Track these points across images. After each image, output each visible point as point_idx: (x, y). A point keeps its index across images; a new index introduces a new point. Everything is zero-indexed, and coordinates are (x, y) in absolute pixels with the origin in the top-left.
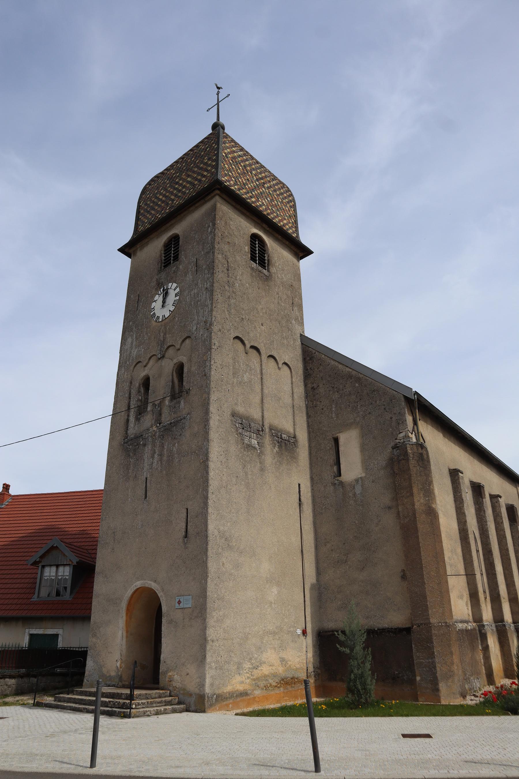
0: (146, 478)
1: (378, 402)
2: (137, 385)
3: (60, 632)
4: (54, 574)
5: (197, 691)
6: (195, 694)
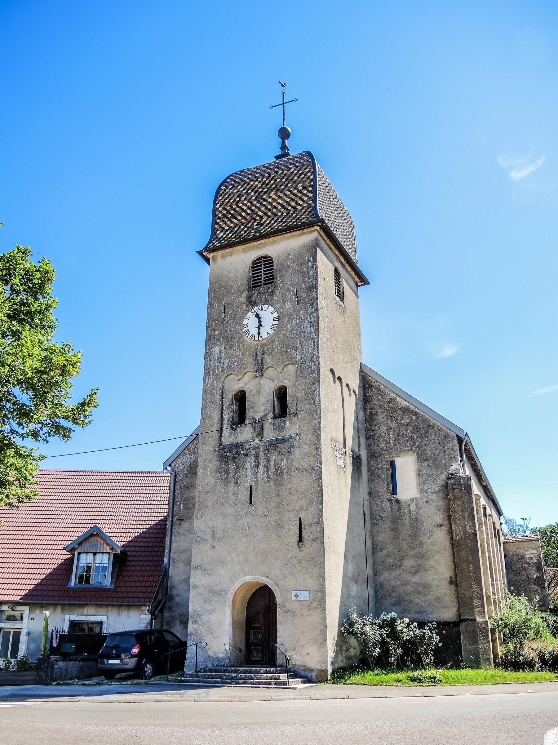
0: (251, 486)
1: (433, 437)
2: (230, 396)
3: (104, 619)
4: (107, 562)
5: (318, 667)
6: (317, 669)
